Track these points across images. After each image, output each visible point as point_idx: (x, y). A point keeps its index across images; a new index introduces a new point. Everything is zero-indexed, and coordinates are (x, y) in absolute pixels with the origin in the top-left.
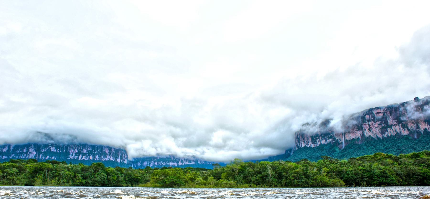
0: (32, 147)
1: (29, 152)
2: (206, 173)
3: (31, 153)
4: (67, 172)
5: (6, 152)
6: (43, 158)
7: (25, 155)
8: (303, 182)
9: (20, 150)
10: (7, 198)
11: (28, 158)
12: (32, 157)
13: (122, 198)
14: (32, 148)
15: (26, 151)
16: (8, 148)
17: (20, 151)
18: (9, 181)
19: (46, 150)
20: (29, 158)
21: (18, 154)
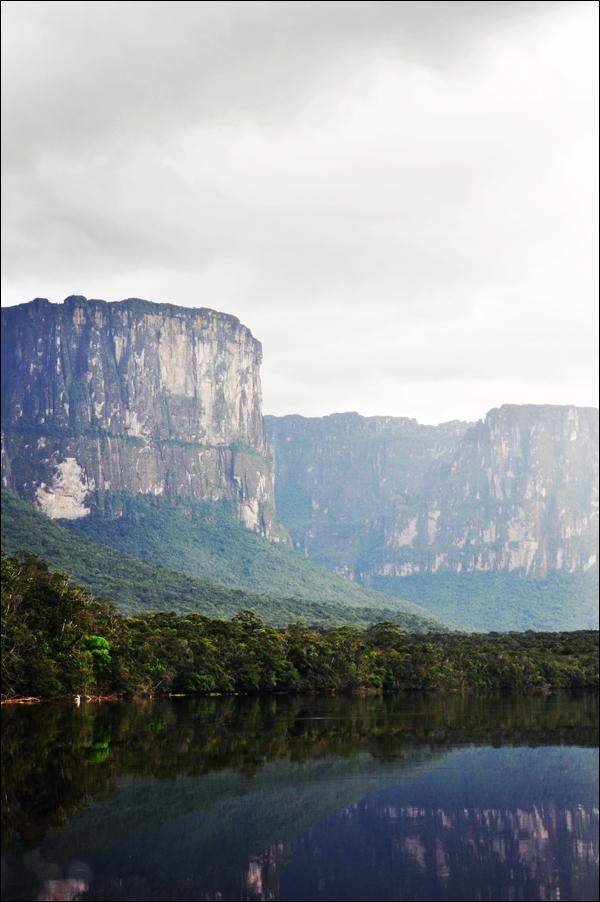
0: (517, 521)
1: (506, 544)
2: (291, 713)
3: (515, 546)
4: (148, 505)
5: (412, 547)
6: (570, 568)
7: (492, 557)
8: (488, 685)
9: (466, 534)
10: (303, 841)
11: (506, 567)
12: (522, 564)
13: (414, 420)
14: (517, 526)
15: (494, 541)
16: (417, 530)
17: (468, 542)
18: (68, 675)
19: (579, 531)
20: (511, 568)
21: (463, 553)
